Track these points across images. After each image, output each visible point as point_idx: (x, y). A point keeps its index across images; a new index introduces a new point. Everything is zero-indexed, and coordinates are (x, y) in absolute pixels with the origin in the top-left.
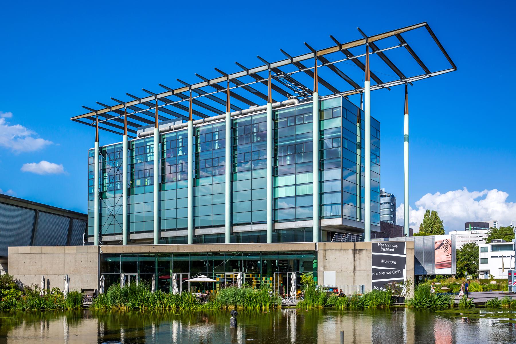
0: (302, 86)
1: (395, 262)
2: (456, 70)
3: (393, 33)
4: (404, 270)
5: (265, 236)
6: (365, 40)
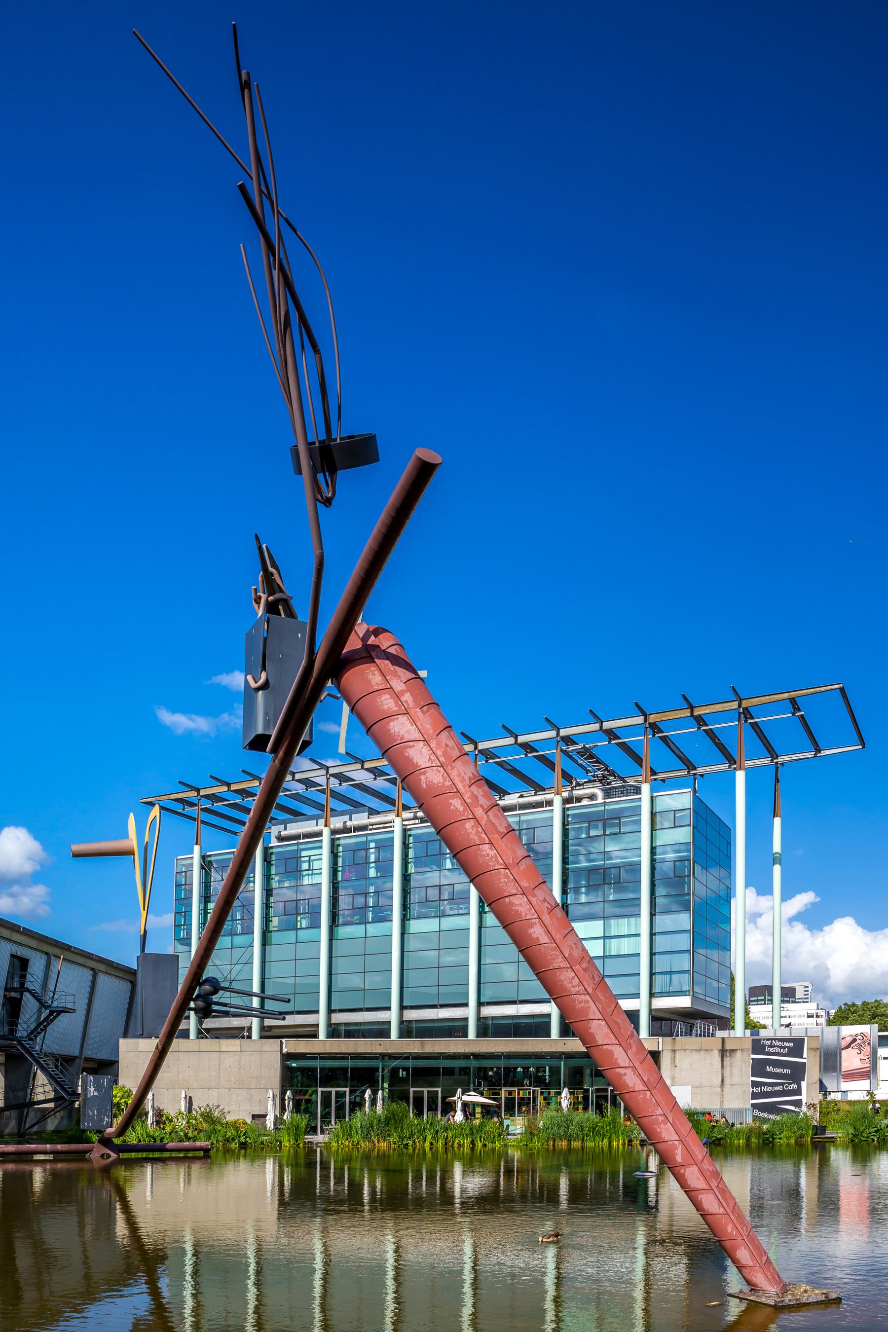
0: (604, 764)
1: (788, 1071)
2: (864, 747)
3: (786, 695)
4: (804, 1084)
5: (549, 1024)
6: (737, 703)
